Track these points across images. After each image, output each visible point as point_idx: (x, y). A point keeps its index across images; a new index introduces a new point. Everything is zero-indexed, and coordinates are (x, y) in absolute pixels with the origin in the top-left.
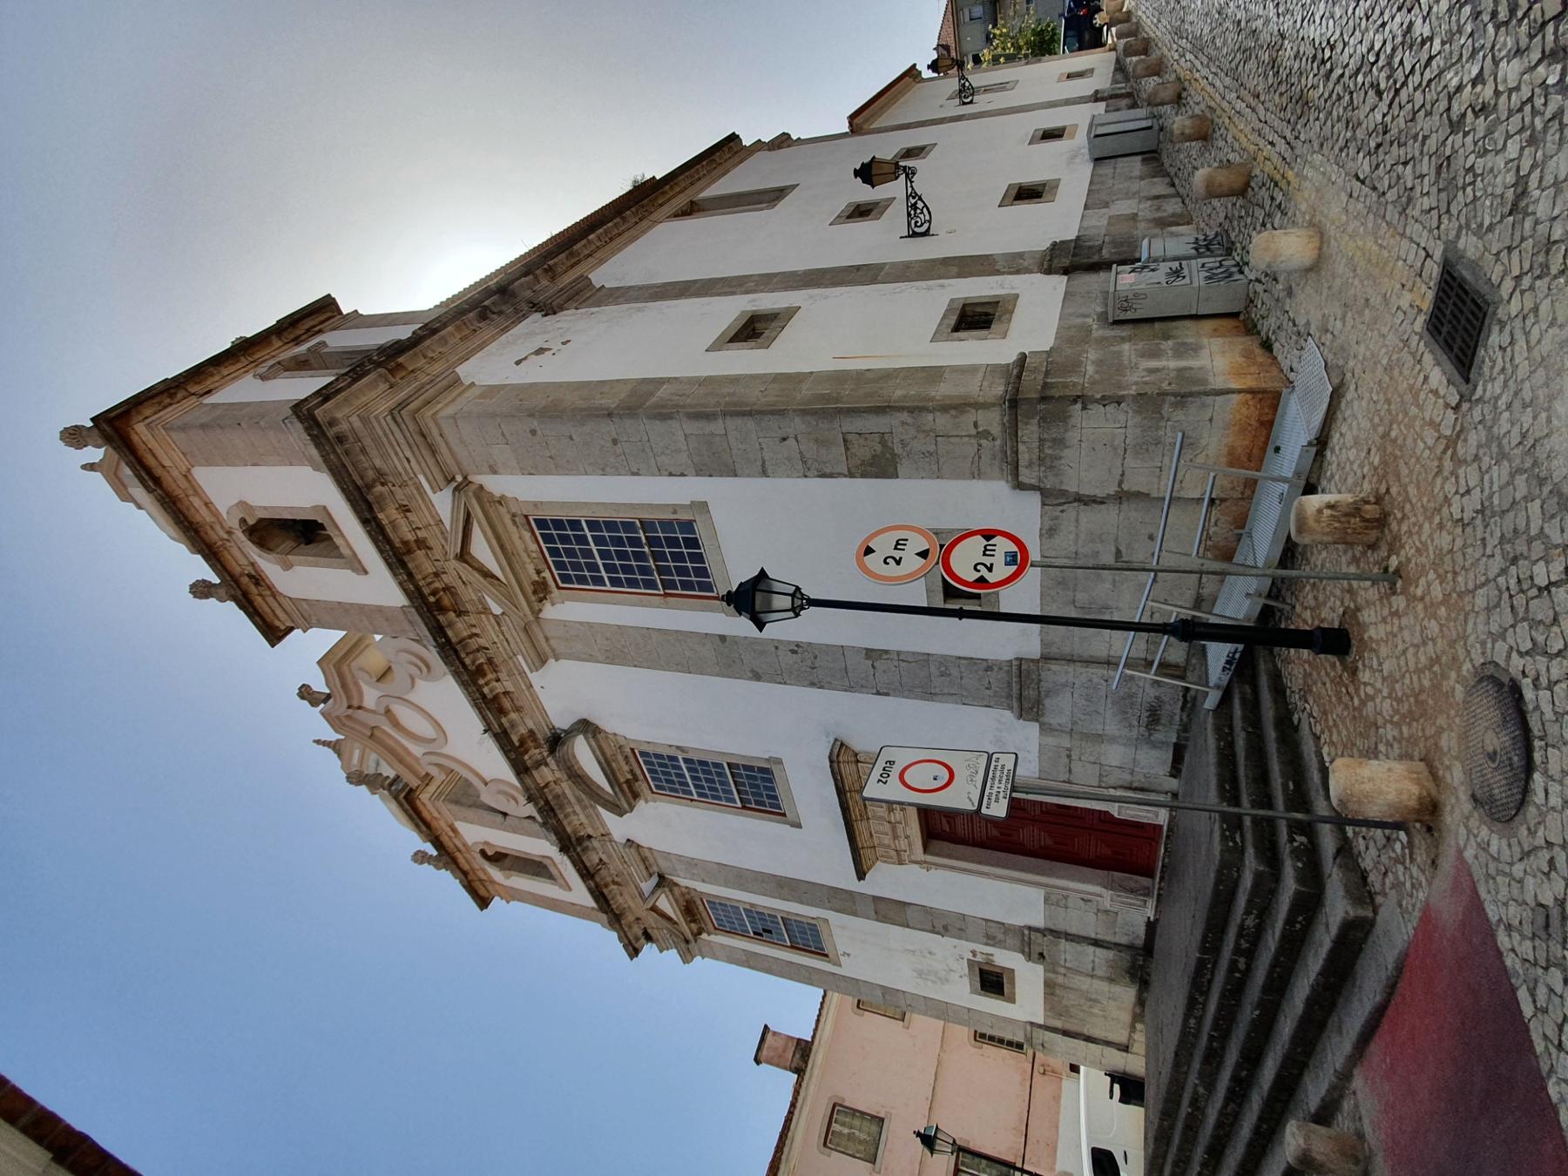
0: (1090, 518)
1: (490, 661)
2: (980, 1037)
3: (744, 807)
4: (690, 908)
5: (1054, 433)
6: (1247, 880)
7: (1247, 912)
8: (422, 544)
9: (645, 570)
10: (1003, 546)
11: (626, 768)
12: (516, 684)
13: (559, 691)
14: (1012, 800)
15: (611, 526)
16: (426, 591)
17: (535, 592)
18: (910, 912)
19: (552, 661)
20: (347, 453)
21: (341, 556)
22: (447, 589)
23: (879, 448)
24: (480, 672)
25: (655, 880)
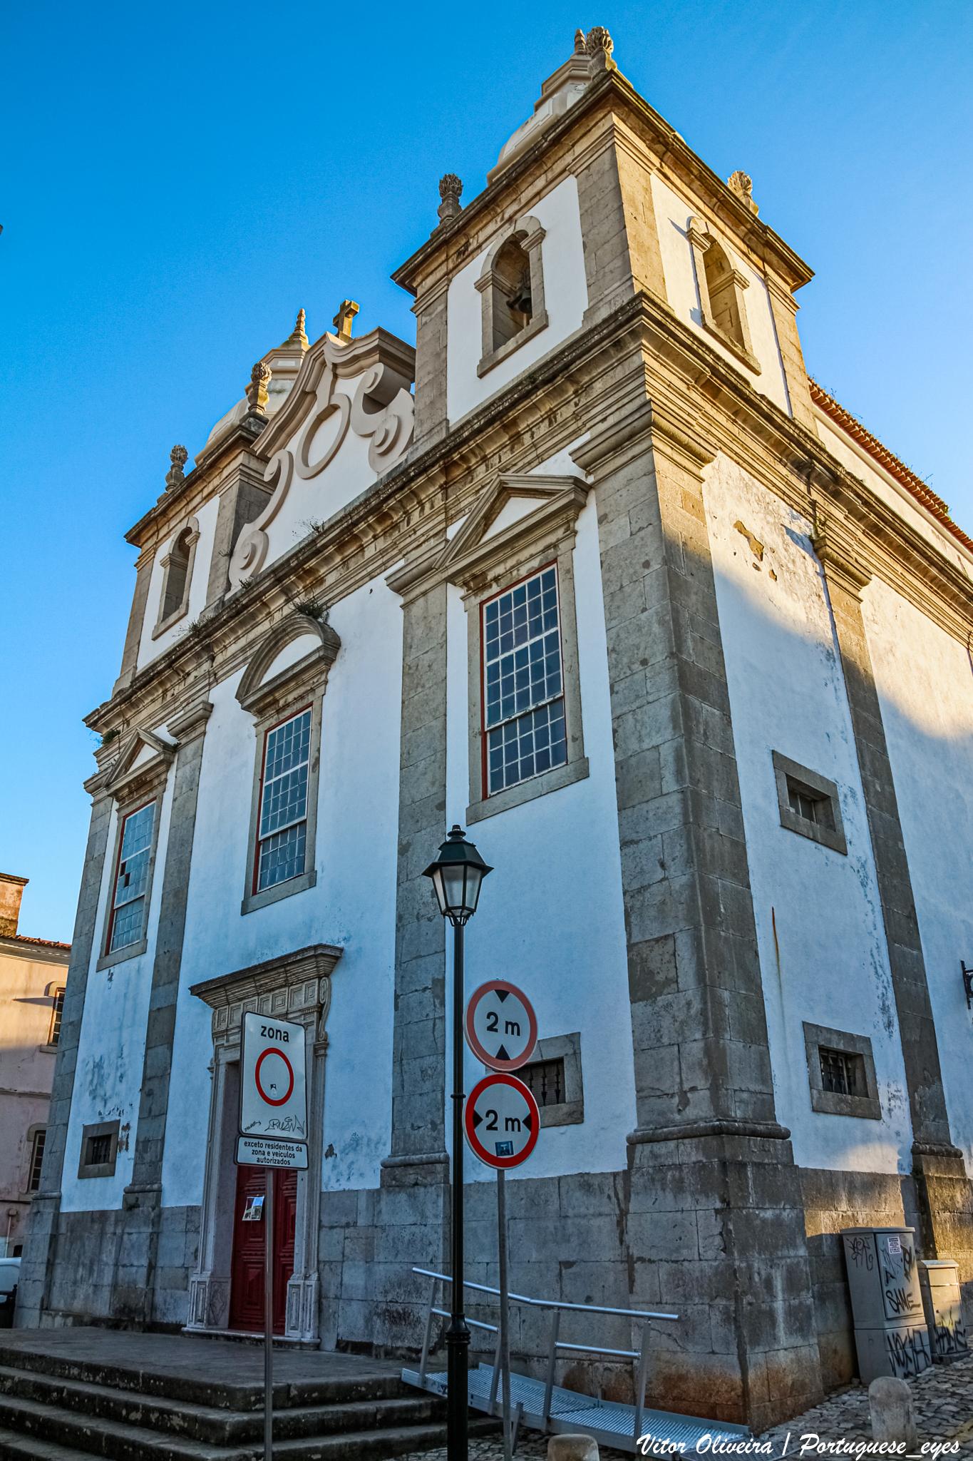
0: (604, 1228)
2: (39, 1137)
3: (259, 844)
4: (145, 784)
5: (689, 1180)
6: (214, 1415)
7: (184, 1417)
10: (519, 1139)
11: (290, 698)
12: (372, 560)
13: (368, 613)
14: (261, 1170)
15: (554, 663)
16: (464, 450)
18: (161, 1050)
19: (401, 601)
21: (497, 346)
22: (470, 471)
23: (660, 977)
25: (172, 741)
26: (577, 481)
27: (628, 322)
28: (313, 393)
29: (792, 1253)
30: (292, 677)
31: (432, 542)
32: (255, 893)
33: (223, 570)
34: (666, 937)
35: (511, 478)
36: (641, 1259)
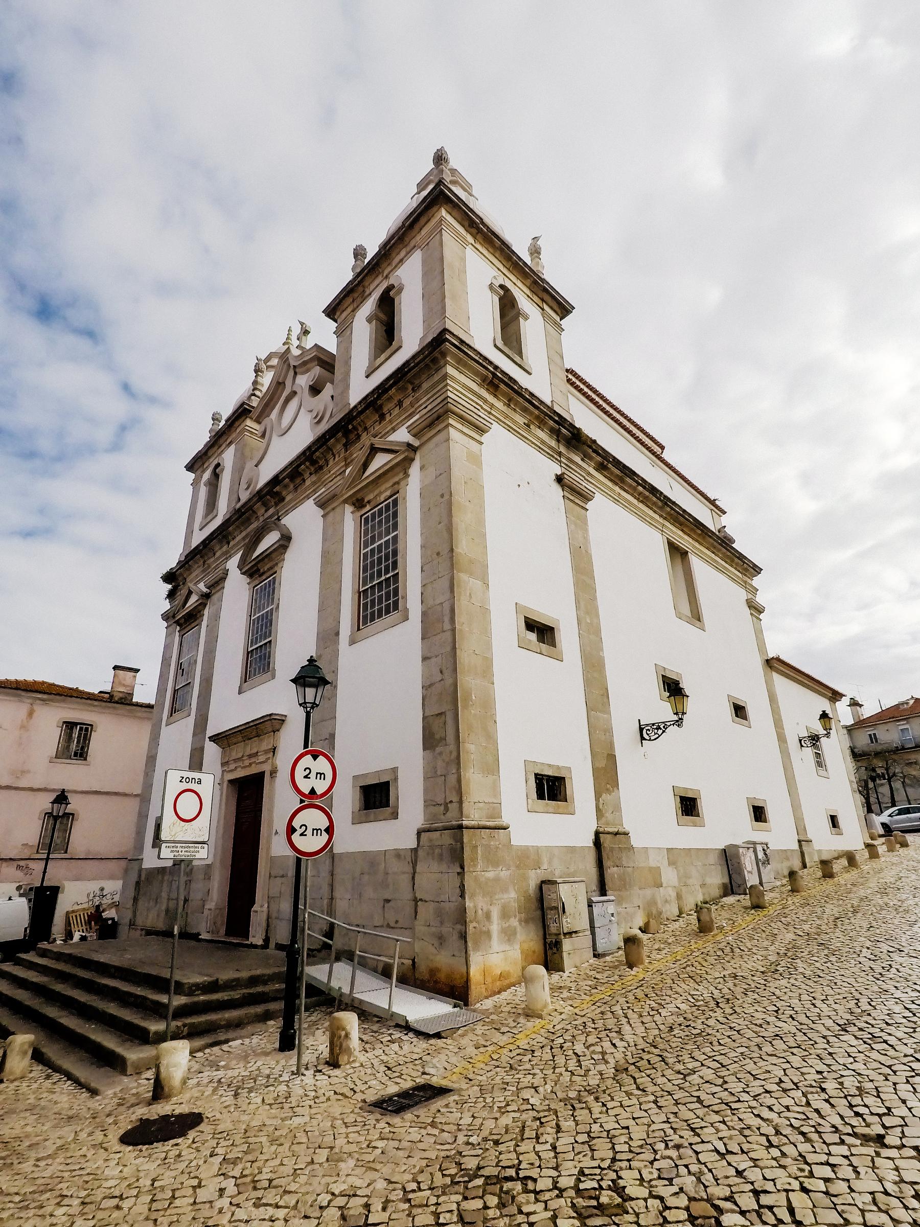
0: (405, 880)
1: (321, 468)
3: (248, 653)
8: (382, 417)
9: (372, 578)
13: (304, 519)
16: (355, 423)
17: (358, 500)
20: (427, 365)
24: (314, 462)
26: (409, 445)
27: (439, 347)
28: (284, 383)
29: (505, 896)
30: (267, 556)
31: (338, 478)
32: (246, 681)
33: (236, 490)
34: (441, 714)
35: (378, 442)
36: (421, 900)
